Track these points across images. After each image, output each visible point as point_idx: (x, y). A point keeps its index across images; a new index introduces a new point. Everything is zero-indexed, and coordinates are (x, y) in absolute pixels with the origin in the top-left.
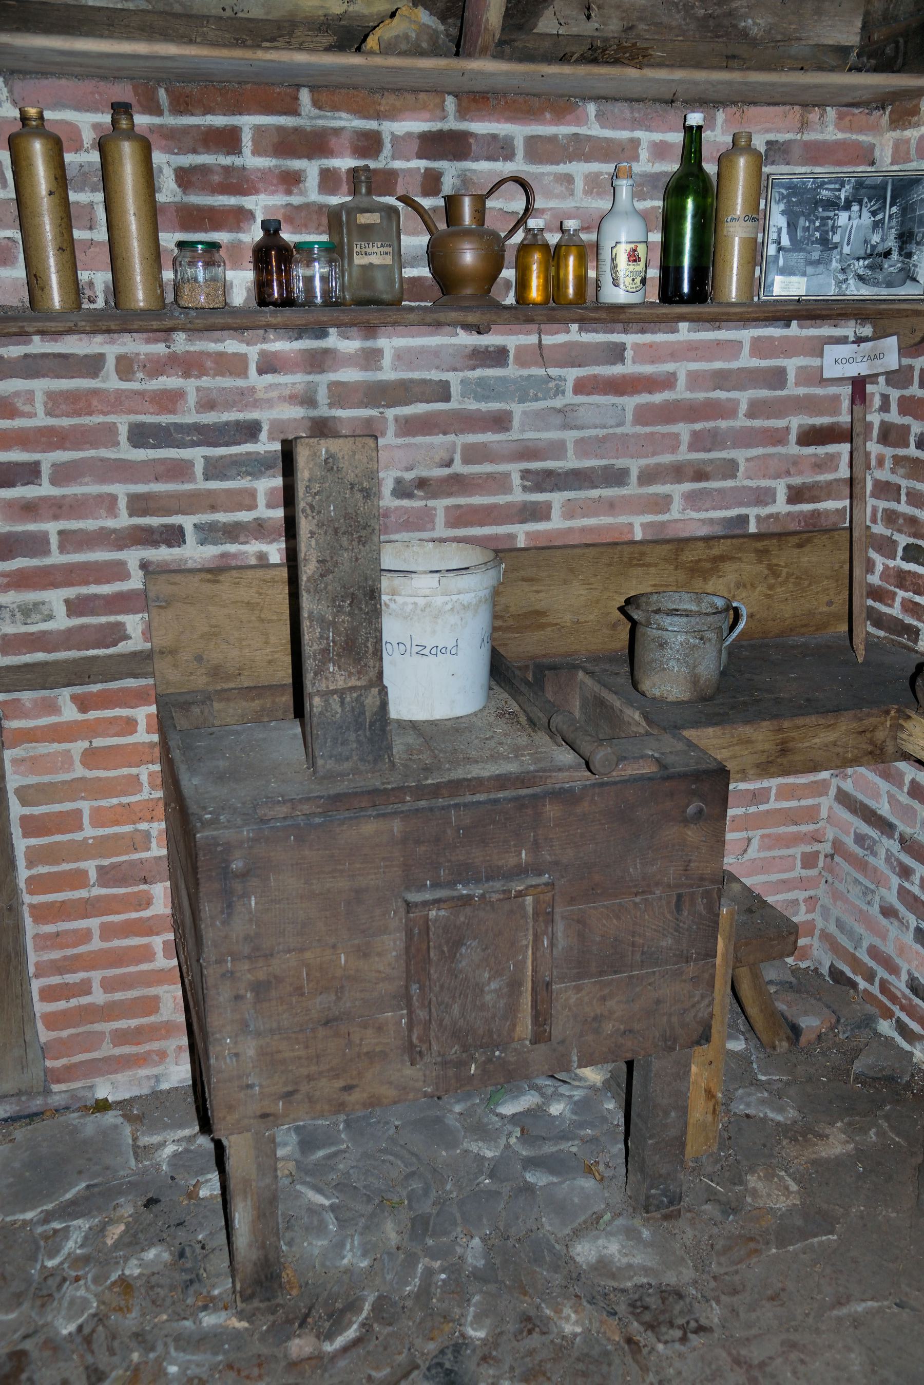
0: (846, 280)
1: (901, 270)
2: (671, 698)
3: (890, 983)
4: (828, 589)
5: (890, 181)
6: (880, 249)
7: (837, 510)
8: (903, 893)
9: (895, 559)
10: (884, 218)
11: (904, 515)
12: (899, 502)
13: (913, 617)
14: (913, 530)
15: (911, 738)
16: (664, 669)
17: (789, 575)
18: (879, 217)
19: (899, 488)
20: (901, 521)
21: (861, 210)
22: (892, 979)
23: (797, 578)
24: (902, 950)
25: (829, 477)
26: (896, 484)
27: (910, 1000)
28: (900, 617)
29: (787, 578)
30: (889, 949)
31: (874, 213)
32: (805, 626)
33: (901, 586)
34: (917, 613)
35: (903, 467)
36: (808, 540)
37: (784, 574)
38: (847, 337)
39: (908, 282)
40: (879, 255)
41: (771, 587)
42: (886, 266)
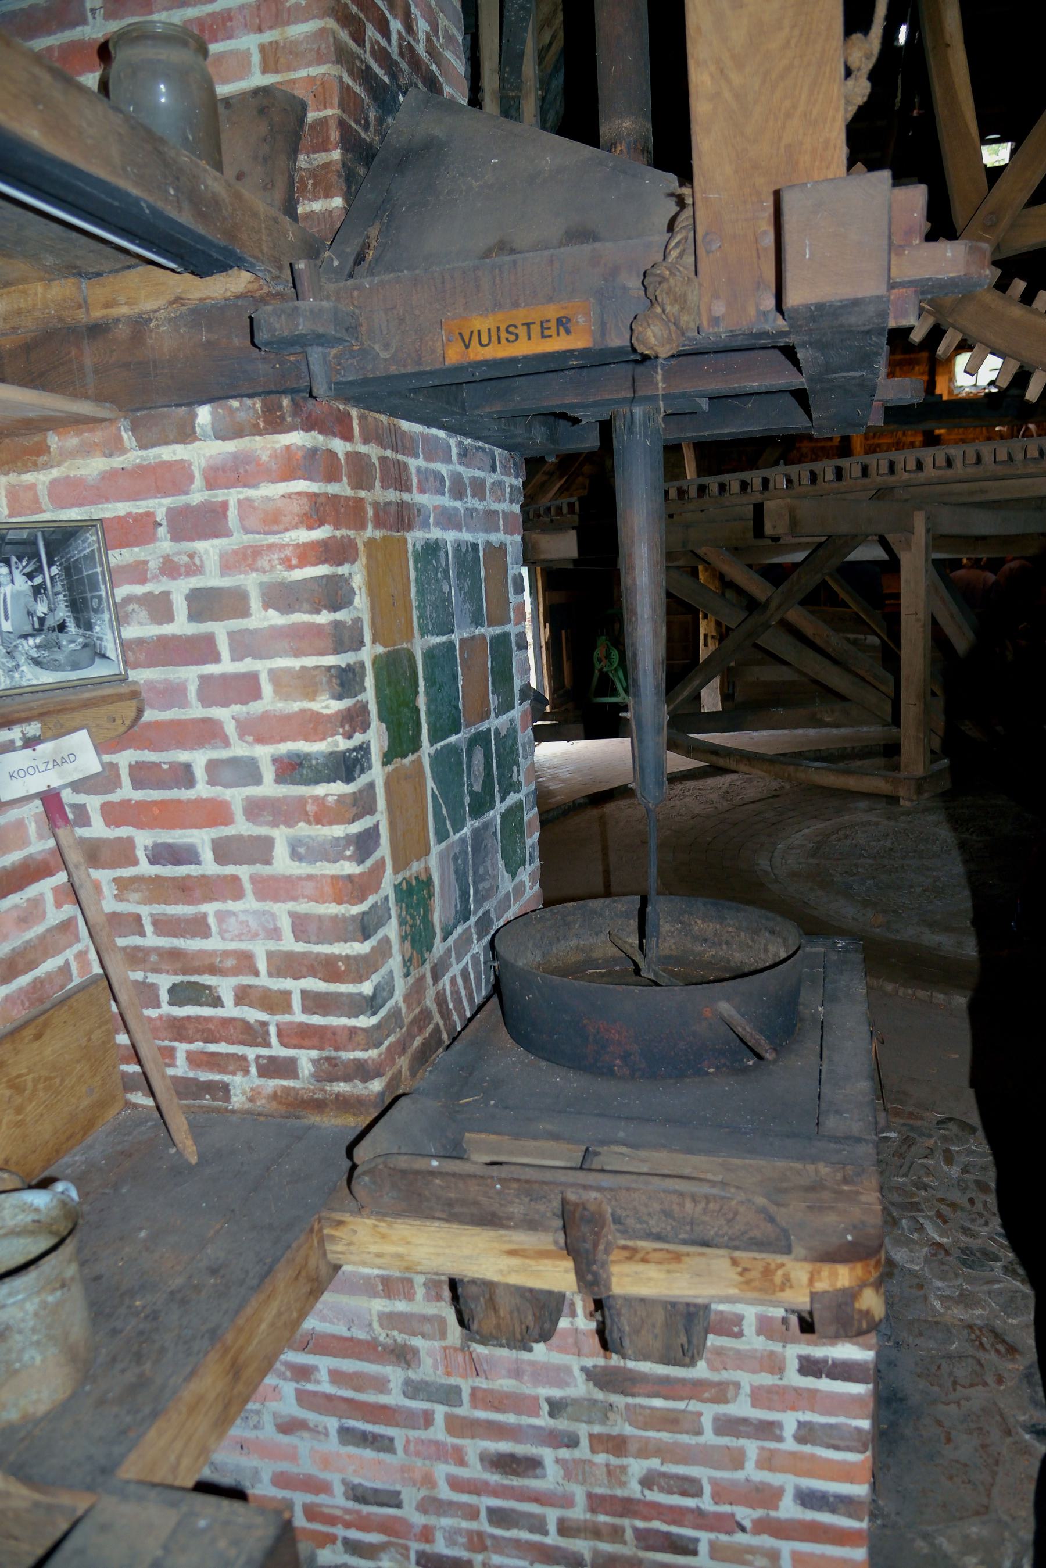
0: (17, 667)
1: (85, 646)
2: (42, 1409)
3: (320, 1505)
4: (83, 1076)
5: (39, 535)
6: (51, 622)
7: (60, 969)
8: (304, 1398)
9: (159, 1006)
10: (44, 582)
11: (157, 950)
12: (143, 934)
13: (212, 1070)
14: (179, 965)
15: (352, 1248)
16: (16, 1372)
17: (36, 1081)
18: (38, 580)
19: (138, 918)
20: (153, 958)
21: (11, 572)
22: (321, 1499)
23: (45, 1081)
24: (326, 1462)
25: (39, 929)
26: (130, 914)
27: (358, 1512)
28: (191, 1075)
29: (35, 1086)
30: (306, 1467)
31: (30, 576)
32: (71, 1136)
33: (181, 1038)
34: (219, 1066)
35: (136, 891)
36: (46, 1024)
37: (30, 1085)
38: (12, 742)
39: (97, 660)
40: (52, 629)
41: (19, 1110)
42: (64, 643)
